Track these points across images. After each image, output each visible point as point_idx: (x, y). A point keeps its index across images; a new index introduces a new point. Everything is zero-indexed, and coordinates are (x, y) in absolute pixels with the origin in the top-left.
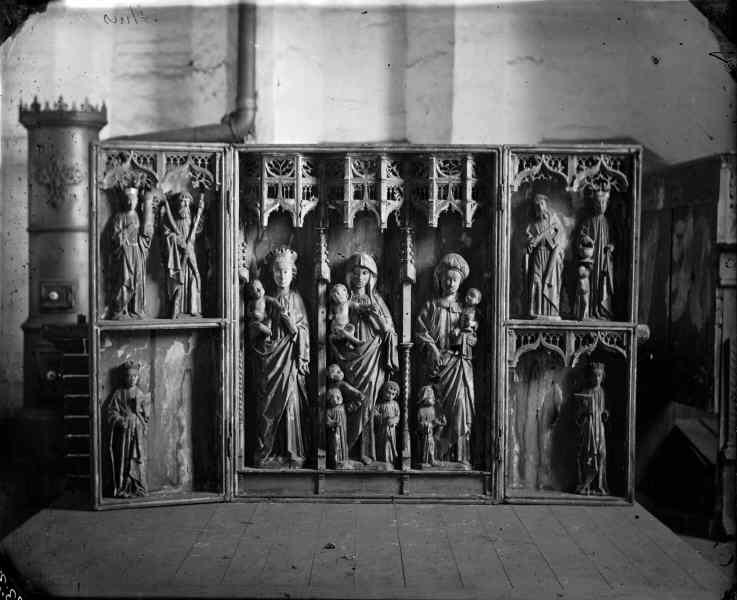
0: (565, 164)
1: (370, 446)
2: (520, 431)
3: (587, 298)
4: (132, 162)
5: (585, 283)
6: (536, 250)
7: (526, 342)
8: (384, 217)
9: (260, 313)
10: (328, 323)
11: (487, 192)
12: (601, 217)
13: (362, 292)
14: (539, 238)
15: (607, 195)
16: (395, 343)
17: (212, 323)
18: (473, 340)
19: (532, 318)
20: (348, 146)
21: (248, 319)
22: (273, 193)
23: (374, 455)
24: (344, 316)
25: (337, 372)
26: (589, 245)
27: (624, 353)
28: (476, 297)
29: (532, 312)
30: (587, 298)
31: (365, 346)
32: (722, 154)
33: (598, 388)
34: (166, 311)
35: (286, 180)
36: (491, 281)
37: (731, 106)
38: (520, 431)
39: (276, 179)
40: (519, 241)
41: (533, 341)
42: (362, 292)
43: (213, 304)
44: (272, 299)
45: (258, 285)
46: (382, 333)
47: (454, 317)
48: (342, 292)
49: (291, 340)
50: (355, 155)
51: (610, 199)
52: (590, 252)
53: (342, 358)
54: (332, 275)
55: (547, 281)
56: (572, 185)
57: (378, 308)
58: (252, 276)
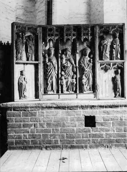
0: (109, 27)
1: (71, 88)
2: (102, 85)
3: (115, 55)
4: (105, 28)
5: (114, 52)
6: (104, 46)
7: (102, 65)
8: (90, 39)
9: (47, 60)
10: (61, 63)
11: (93, 34)
12: (117, 38)
13: (68, 56)
14: (104, 43)
15: (118, 34)
16: (75, 66)
17: (37, 62)
18: (92, 64)
19: (103, 60)
20: (64, 25)
21: (44, 62)
22: (67, 35)
23: (71, 90)
24: (64, 61)
25: (63, 73)
26: (115, 44)
27: (123, 67)
28: (92, 56)
29: (103, 59)
30: (115, 55)
31: (69, 67)
32: (40, 26)
33: (119, 75)
34: (28, 60)
35: (87, 32)
36: (95, 53)
37: (54, 5)
38: (102, 85)
39: (50, 33)
40: (100, 45)
41: (103, 65)
42: (68, 56)
43: (37, 59)
44: (49, 58)
45: (46, 55)
46: (72, 64)
47: (88, 60)
48: (64, 56)
49: (54, 66)
50: (122, 27)
51: (119, 35)
52: (115, 46)
53: (64, 70)
54: (62, 52)
55: (106, 52)
56: (111, 32)
57: (71, 59)
58: (45, 53)
